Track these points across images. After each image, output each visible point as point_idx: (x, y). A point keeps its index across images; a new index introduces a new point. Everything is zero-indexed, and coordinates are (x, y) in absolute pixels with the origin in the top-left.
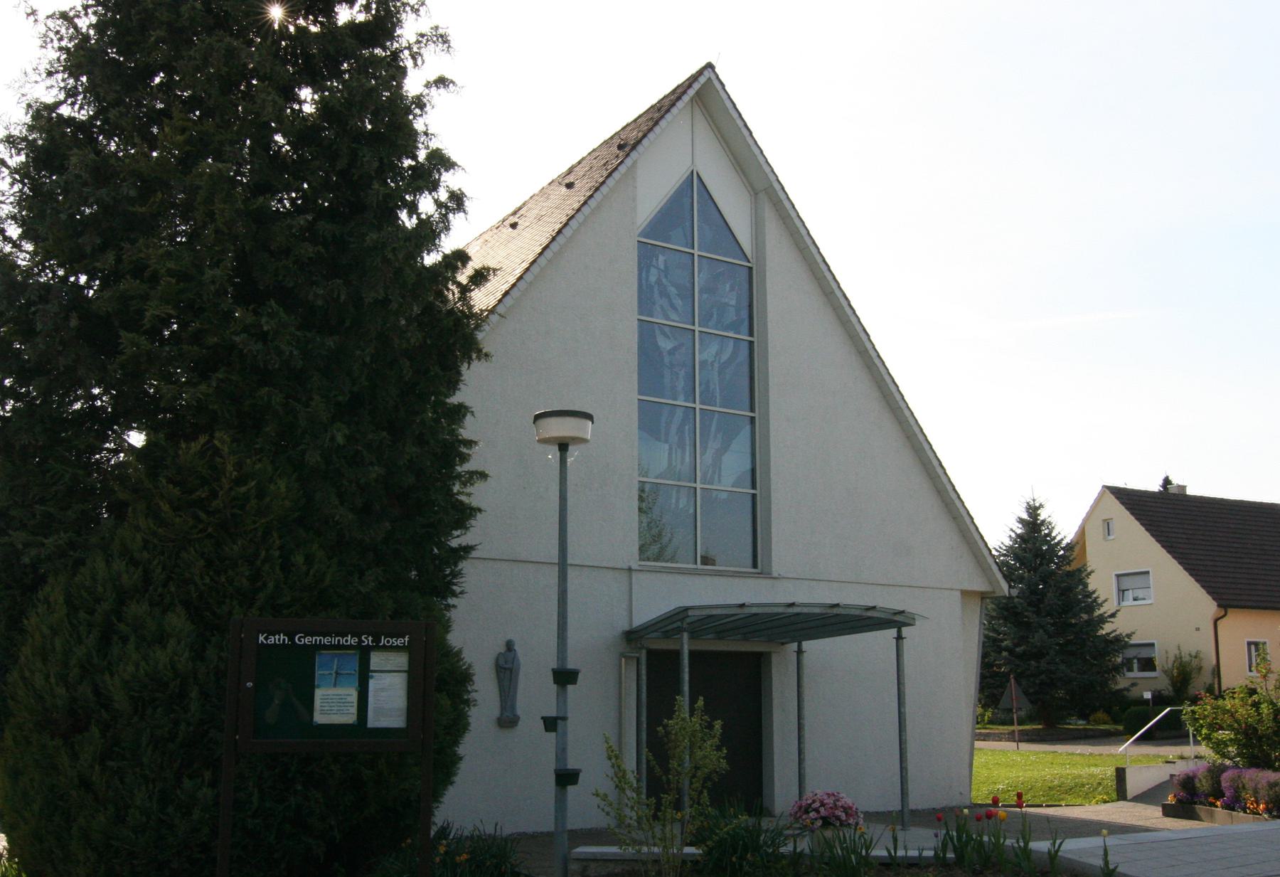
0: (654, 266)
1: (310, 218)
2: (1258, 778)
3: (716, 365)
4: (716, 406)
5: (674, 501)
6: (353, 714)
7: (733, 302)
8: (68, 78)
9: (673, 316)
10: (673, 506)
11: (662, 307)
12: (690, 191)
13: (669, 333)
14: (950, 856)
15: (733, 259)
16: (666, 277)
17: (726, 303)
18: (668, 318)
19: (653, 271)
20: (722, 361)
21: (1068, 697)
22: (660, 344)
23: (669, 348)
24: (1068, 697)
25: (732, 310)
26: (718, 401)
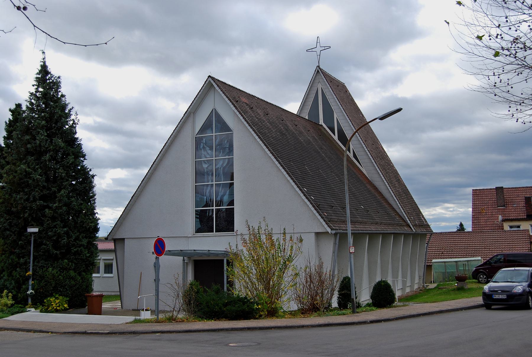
0: (202, 143)
1: (74, 250)
2: (88, 278)
3: (222, 168)
4: (221, 181)
5: (208, 214)
6: (188, 248)
7: (228, 146)
8: (4, 283)
9: (208, 156)
10: (208, 215)
11: (204, 155)
12: (216, 163)
13: (207, 162)
14: (461, 269)
15: (228, 132)
16: (206, 145)
17: (225, 147)
18: (206, 158)
19: (202, 144)
20: (224, 166)
21: (62, 288)
22: (203, 166)
23: (206, 167)
24: (62, 288)
25: (227, 149)
26: (222, 180)
